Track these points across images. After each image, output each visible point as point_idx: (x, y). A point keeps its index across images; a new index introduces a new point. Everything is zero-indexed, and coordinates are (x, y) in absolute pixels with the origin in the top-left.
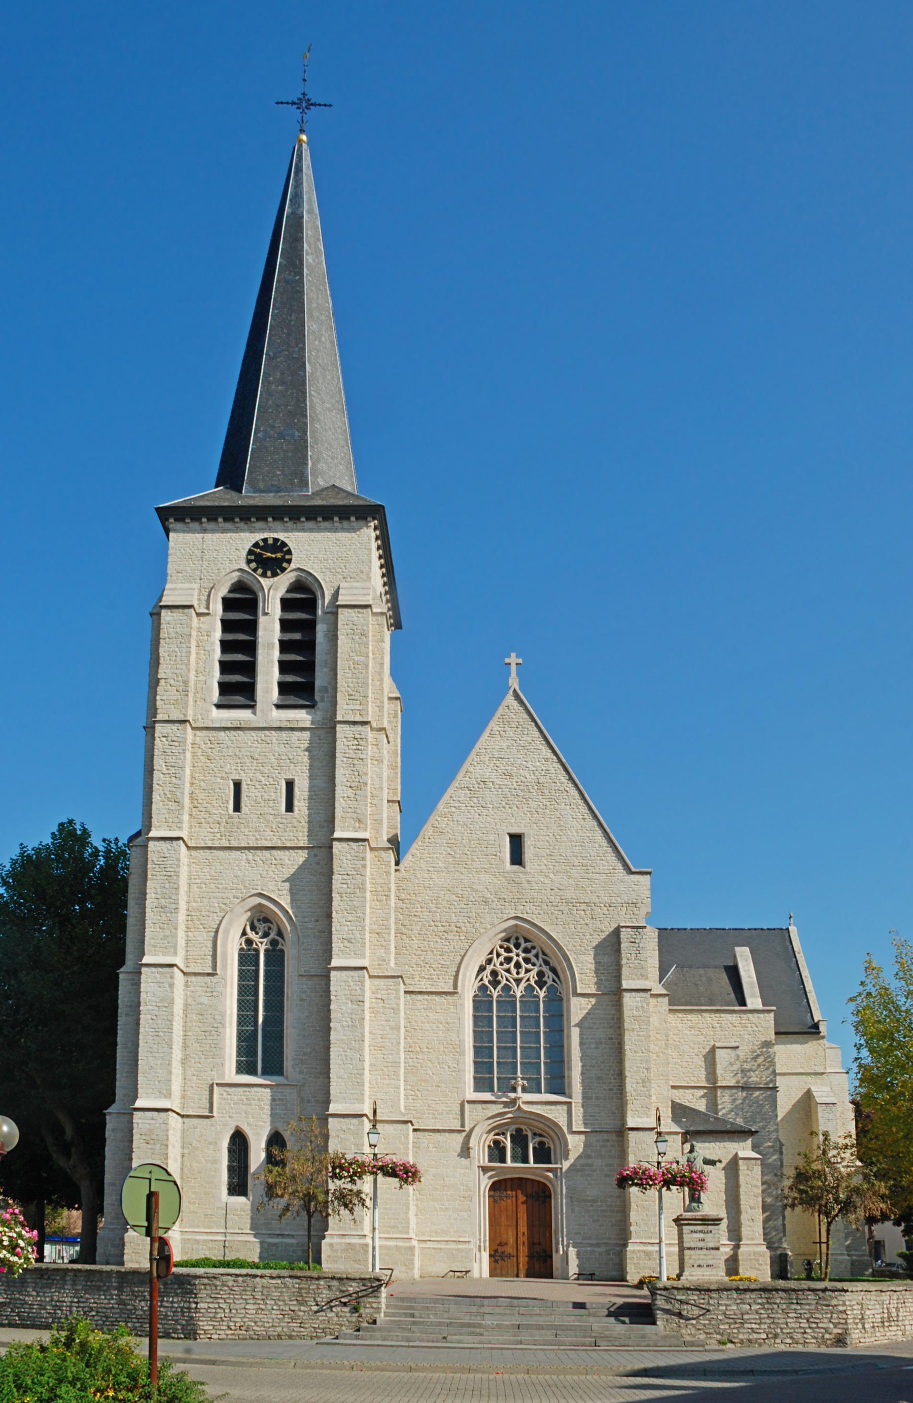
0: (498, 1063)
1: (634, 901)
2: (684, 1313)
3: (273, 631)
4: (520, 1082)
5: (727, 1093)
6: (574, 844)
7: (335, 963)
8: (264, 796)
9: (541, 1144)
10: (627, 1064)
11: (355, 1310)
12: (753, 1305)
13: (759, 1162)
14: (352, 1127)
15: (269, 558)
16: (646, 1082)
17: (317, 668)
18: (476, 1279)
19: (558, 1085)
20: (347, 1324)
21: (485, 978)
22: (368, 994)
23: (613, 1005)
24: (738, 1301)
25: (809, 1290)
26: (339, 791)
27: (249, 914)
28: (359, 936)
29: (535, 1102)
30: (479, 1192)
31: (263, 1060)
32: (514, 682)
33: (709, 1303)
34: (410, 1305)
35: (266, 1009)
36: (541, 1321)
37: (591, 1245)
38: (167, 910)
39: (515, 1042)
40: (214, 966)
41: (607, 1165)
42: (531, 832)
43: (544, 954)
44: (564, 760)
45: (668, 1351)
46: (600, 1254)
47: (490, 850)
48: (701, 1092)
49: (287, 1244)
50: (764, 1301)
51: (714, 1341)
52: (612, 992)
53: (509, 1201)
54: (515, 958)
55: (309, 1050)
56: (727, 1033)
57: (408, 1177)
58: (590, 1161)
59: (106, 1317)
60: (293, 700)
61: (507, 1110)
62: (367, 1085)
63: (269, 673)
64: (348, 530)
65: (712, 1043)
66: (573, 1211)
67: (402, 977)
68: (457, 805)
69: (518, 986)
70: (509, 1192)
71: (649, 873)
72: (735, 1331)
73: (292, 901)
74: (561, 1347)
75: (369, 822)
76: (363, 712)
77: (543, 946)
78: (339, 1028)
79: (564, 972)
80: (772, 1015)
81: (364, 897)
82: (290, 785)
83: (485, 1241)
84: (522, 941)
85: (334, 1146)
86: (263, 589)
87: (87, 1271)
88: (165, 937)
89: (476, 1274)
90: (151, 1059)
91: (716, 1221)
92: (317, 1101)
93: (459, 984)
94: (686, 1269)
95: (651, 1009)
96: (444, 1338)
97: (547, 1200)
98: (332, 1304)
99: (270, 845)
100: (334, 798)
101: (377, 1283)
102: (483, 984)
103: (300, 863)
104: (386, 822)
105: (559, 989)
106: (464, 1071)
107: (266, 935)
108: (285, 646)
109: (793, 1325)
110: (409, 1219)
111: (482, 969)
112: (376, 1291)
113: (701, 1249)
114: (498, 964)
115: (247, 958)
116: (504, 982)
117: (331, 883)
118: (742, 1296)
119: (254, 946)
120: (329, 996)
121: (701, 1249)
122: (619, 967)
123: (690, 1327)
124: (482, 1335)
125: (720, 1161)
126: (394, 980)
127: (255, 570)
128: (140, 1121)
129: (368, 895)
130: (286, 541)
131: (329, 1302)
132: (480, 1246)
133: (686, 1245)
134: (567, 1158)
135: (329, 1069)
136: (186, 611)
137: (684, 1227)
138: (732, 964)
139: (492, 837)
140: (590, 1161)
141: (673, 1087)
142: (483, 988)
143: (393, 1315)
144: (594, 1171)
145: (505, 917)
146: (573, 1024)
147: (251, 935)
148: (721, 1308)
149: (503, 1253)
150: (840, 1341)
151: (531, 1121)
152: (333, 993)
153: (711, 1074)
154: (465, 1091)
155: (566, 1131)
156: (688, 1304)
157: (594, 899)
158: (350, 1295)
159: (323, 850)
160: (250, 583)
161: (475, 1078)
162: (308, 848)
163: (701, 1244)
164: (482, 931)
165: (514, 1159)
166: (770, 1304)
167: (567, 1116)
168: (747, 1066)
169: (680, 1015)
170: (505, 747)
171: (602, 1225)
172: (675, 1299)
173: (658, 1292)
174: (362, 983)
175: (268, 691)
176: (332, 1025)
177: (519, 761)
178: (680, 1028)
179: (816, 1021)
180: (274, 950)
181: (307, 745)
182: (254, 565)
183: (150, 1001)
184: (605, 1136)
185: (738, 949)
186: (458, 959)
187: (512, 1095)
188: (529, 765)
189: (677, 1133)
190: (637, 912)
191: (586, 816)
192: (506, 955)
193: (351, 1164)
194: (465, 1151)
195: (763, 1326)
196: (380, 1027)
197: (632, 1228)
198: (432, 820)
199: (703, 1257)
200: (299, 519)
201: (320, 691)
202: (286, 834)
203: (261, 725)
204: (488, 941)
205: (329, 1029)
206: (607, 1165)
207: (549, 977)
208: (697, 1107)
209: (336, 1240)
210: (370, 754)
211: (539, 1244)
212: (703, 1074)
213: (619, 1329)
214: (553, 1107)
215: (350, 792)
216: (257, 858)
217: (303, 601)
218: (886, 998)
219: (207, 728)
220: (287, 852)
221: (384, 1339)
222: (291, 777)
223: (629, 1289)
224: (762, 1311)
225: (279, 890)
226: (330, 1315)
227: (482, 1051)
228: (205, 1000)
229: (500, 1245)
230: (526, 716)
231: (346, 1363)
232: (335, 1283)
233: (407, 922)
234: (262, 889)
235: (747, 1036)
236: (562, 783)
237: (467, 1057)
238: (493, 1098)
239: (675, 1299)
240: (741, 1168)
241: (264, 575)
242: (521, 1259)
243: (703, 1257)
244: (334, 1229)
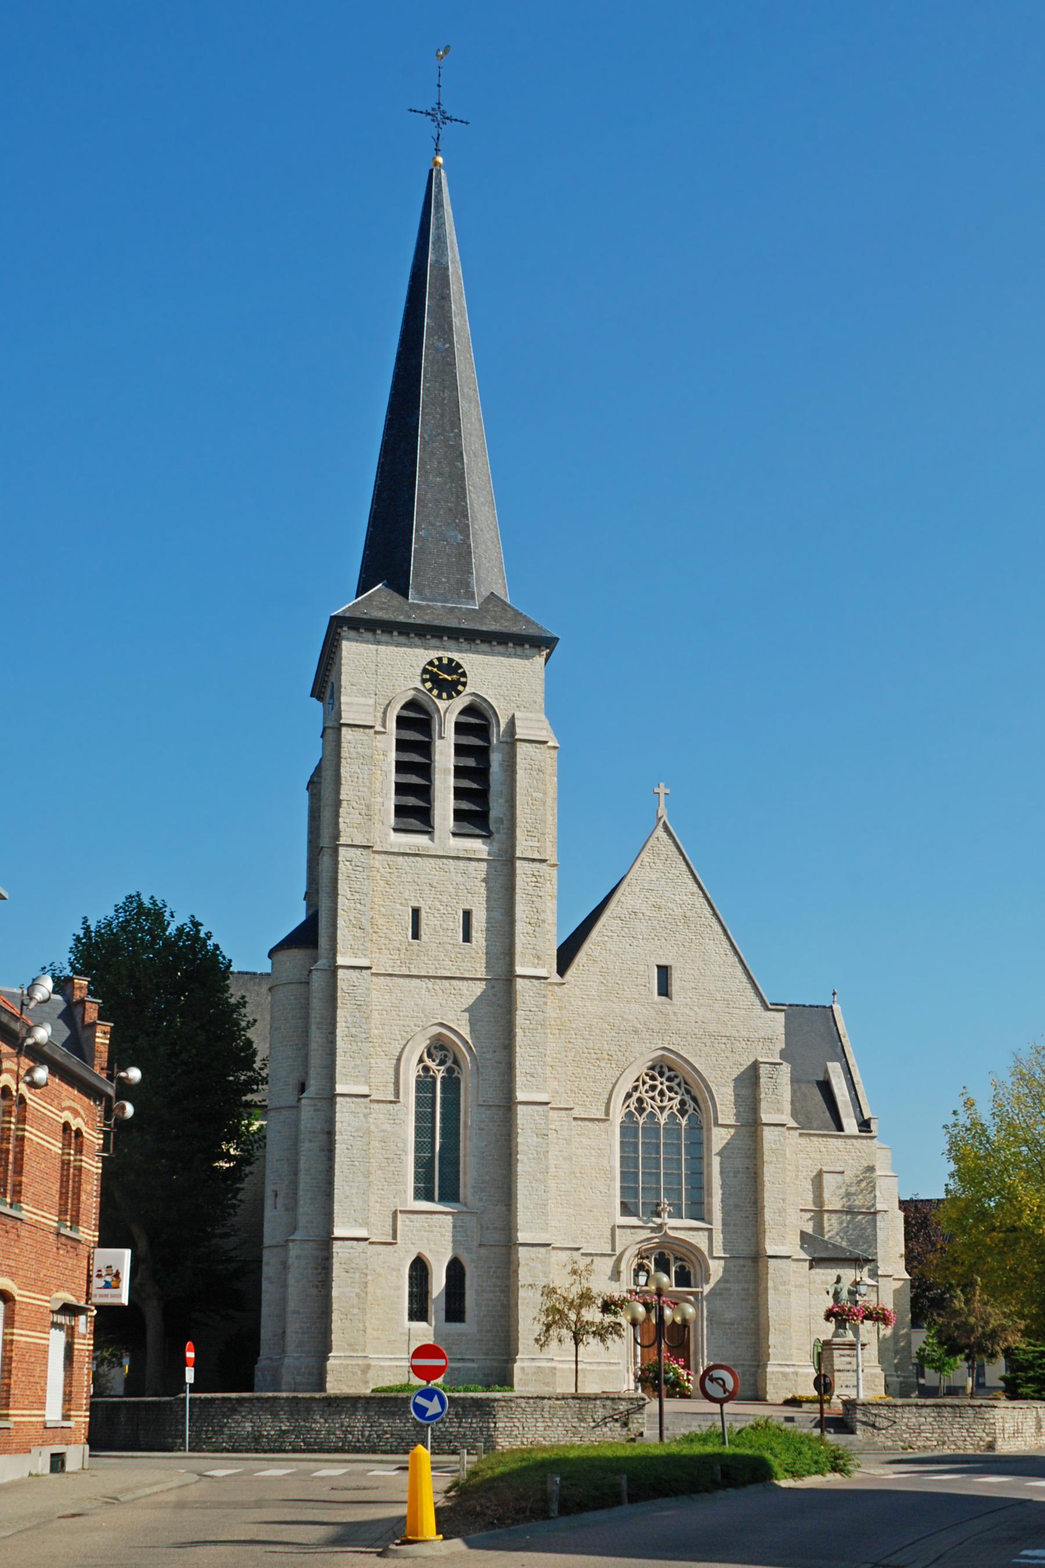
2: (877, 1424)
5: (834, 1216)
8: (440, 925)
9: (682, 1268)
11: (625, 1425)
14: (540, 1256)
15: (445, 679)
16: (781, 1211)
19: (698, 1210)
25: (969, 1406)
26: (520, 927)
27: (428, 1042)
28: (540, 1071)
29: (679, 1227)
35: (442, 1136)
38: (358, 1039)
40: (397, 1094)
41: (743, 1289)
43: (686, 1083)
44: (709, 896)
47: (640, 981)
48: (809, 1215)
49: (469, 1369)
52: (751, 1124)
54: (660, 1087)
58: (728, 1285)
59: (402, 1439)
60: (468, 828)
61: (654, 1235)
63: (445, 799)
64: (521, 657)
65: (819, 1167)
66: (713, 1334)
73: (471, 1031)
76: (541, 850)
78: (526, 1160)
79: (705, 1102)
82: (467, 915)
84: (666, 1069)
86: (439, 711)
87: (381, 1398)
88: (356, 1066)
90: (346, 1188)
92: (496, 1228)
102: (630, 1111)
107: (442, 1063)
108: (460, 772)
111: (629, 1096)
115: (424, 1085)
116: (650, 1109)
127: (430, 690)
128: (339, 1250)
130: (461, 662)
134: (707, 1282)
136: (367, 731)
137: (835, 1352)
139: (642, 968)
140: (728, 1285)
142: (629, 1115)
145: (653, 1047)
146: (714, 1152)
147: (428, 1062)
150: (991, 1446)
151: (675, 1247)
153: (818, 1198)
157: (734, 1033)
160: (425, 704)
163: (848, 1367)
167: (708, 1239)
168: (853, 1190)
175: (445, 818)
179: (866, 1118)
180: (450, 1077)
181: (484, 876)
182: (429, 685)
183: (346, 1130)
184: (741, 1262)
185: (829, 1064)
186: (610, 1086)
187: (658, 1221)
188: (677, 898)
189: (805, 1260)
192: (652, 1083)
200: (474, 641)
201: (496, 822)
203: (439, 853)
206: (743, 1289)
207: (690, 1105)
209: (526, 1364)
212: (810, 1197)
214: (695, 1233)
216: (437, 987)
217: (477, 722)
218: (977, 1129)
219: (386, 853)
220: (465, 983)
226: (605, 1429)
227: (628, 1176)
228: (388, 1127)
230: (674, 849)
232: (609, 1403)
238: (641, 1224)
241: (439, 696)
244: (523, 1353)
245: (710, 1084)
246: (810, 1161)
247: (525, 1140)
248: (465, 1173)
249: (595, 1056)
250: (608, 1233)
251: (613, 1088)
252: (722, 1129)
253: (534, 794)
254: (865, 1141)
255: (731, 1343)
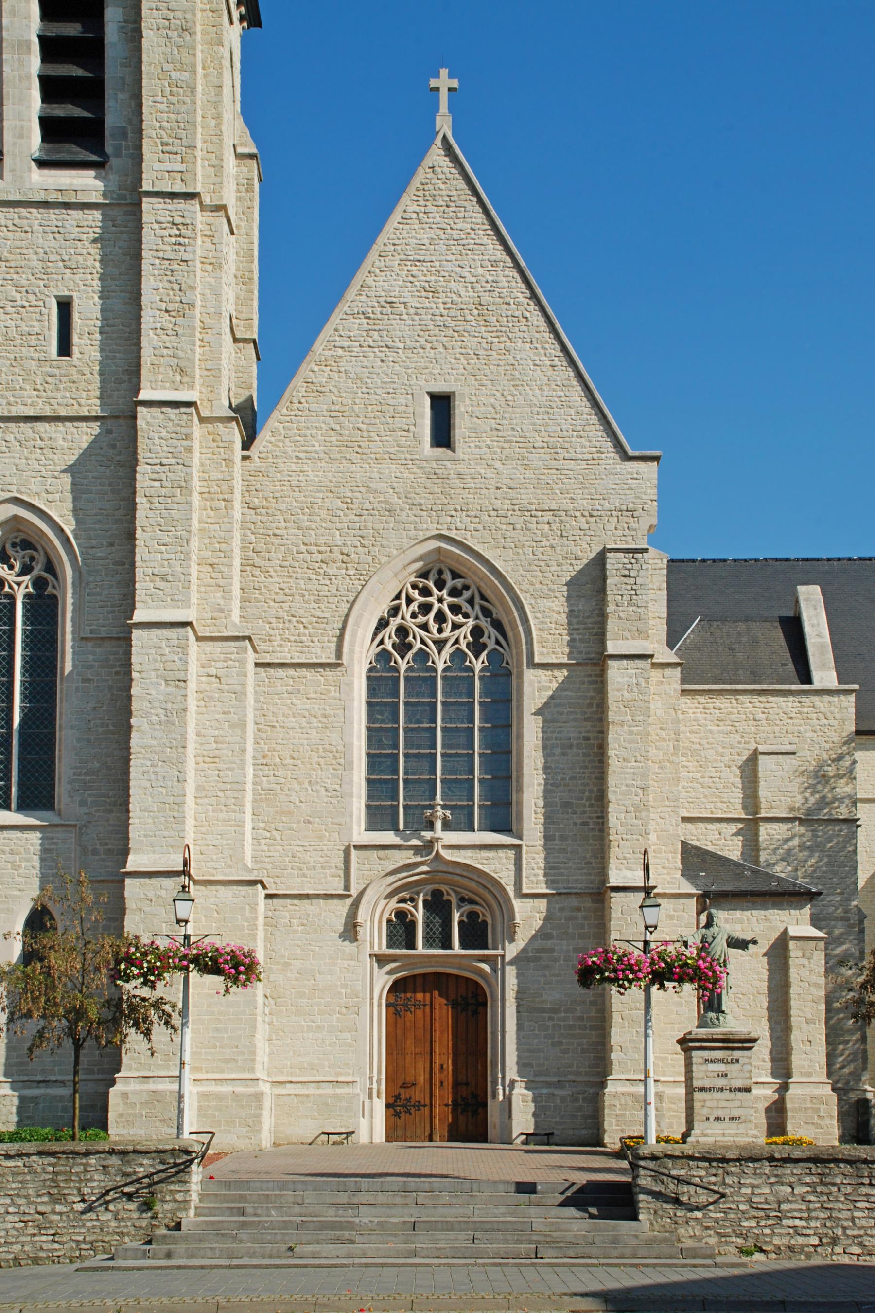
0: (406, 781)
1: (631, 506)
3: (28, 17)
4: (440, 812)
6: (535, 410)
7: (139, 616)
9: (473, 915)
10: (612, 781)
11: (147, 1206)
12: (795, 1186)
13: (822, 944)
14: (163, 893)
17: (108, 92)
18: (364, 1147)
20: (132, 1231)
21: (386, 640)
22: (193, 668)
23: (591, 683)
24: (773, 1180)
28: (179, 569)
29: (464, 846)
30: (372, 999)
31: (20, 785)
32: (444, 124)
33: (724, 1183)
34: (240, 1193)
36: (451, 1214)
37: (548, 1084)
39: (434, 746)
42: (466, 390)
43: (483, 597)
44: (523, 264)
45: (654, 1266)
46: (563, 1099)
47: (399, 423)
48: (734, 828)
50: (816, 1179)
51: (732, 1249)
52: (591, 660)
53: (419, 1013)
55: (97, 765)
56: (777, 729)
57: (239, 973)
58: (549, 944)
61: (419, 859)
62: (190, 822)
63: (23, 99)
65: (753, 746)
67: (249, 638)
68: (346, 344)
69: (439, 652)
70: (420, 996)
71: (656, 459)
72: (767, 1231)
74: (480, 1261)
75: (198, 372)
76: (186, 177)
77: (482, 584)
79: (514, 628)
80: (852, 698)
81: (189, 503)
82: (65, 307)
83: (379, 1081)
84: (447, 576)
85: (132, 925)
89: (363, 1137)
91: (747, 1043)
92: (109, 852)
93: (345, 650)
94: (696, 1124)
95: (652, 689)
96: (291, 1249)
97: (481, 1009)
98: (108, 1198)
99: (32, 414)
100: (139, 331)
101: (185, 1157)
102: (384, 650)
103: (85, 445)
104: (233, 374)
105: (506, 655)
106: (351, 795)
109: (864, 1223)
110: (254, 1046)
111: (383, 624)
112: (182, 1171)
113: (722, 1090)
114: (408, 617)
116: (418, 645)
117: (135, 479)
118: (779, 1171)
119: (7, 589)
120: (130, 673)
121: (722, 1090)
122: (602, 618)
123: (692, 1223)
124: (352, 1242)
125: (755, 942)
126: (237, 644)
129: (196, 500)
131: (103, 1195)
132: (371, 1089)
133: (696, 1083)
134: (512, 940)
135: (129, 796)
137: (695, 1053)
138: (791, 614)
140: (549, 944)
141: (685, 820)
142: (383, 656)
143: (211, 1212)
144: (555, 960)
145: (421, 535)
148: (743, 1191)
149: (408, 1100)
151: (457, 878)
152: (135, 667)
154: (351, 828)
155: (512, 894)
156: (689, 1183)
157: (566, 504)
158: (138, 1180)
159: (122, 421)
161: (368, 807)
162: (96, 418)
163: (721, 1082)
164: (384, 559)
165: (429, 942)
166: (826, 1184)
167: (519, 867)
169: (702, 699)
170: (426, 242)
171: (565, 1052)
172: (669, 1176)
173: (642, 1163)
174: (184, 649)
175: (23, 134)
176: (133, 721)
177: (449, 267)
178: (702, 722)
184: (574, 902)
187: (428, 835)
189: (689, 896)
190: (636, 526)
191: (556, 362)
193: (145, 954)
194: (351, 931)
195: (813, 1224)
196: (214, 723)
197: (613, 1056)
198: (304, 370)
199: (725, 1104)
202: (59, 395)
203: (12, 198)
204: (393, 576)
205: (130, 727)
206: (576, 950)
208: (725, 854)
209: (133, 1086)
210: (199, 252)
211: (467, 1084)
213: (577, 1224)
214: (491, 854)
215: (166, 321)
221: (191, 1256)
222: (67, 293)
223: (603, 1158)
224: (812, 1198)
225: (48, 492)
226: (106, 1217)
227: (380, 762)
229: (404, 1086)
230: (462, 185)
231: (109, 1302)
232: (114, 1161)
233: (261, 546)
234: (19, 491)
235: (809, 734)
236: (519, 304)
237: (355, 772)
238: (397, 840)
239: (669, 1176)
240: (792, 954)
242: (437, 1110)
243: (725, 1104)
244: (130, 1069)
245: (521, 596)
246: (738, 737)
247: (146, 690)
248: (60, 758)
249: (320, 557)
250: (338, 859)
251: (350, 609)
252: (540, 672)
253: (174, 74)
254: (835, 699)
255: (553, 1044)
